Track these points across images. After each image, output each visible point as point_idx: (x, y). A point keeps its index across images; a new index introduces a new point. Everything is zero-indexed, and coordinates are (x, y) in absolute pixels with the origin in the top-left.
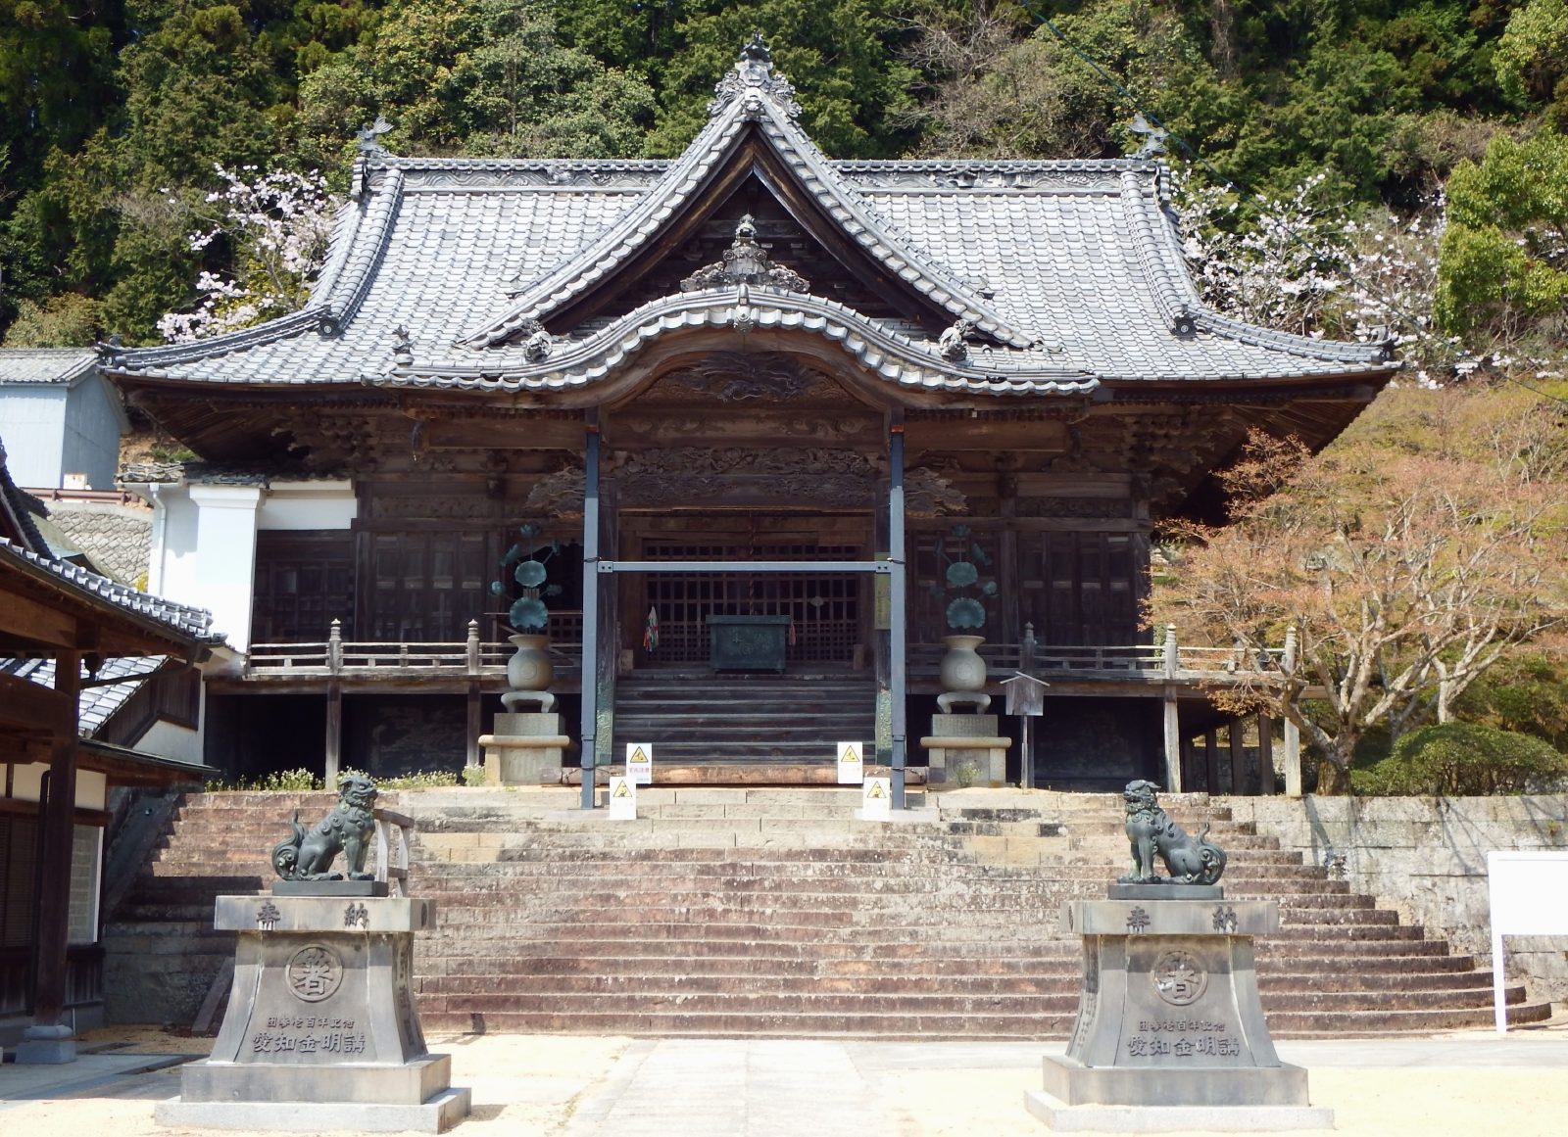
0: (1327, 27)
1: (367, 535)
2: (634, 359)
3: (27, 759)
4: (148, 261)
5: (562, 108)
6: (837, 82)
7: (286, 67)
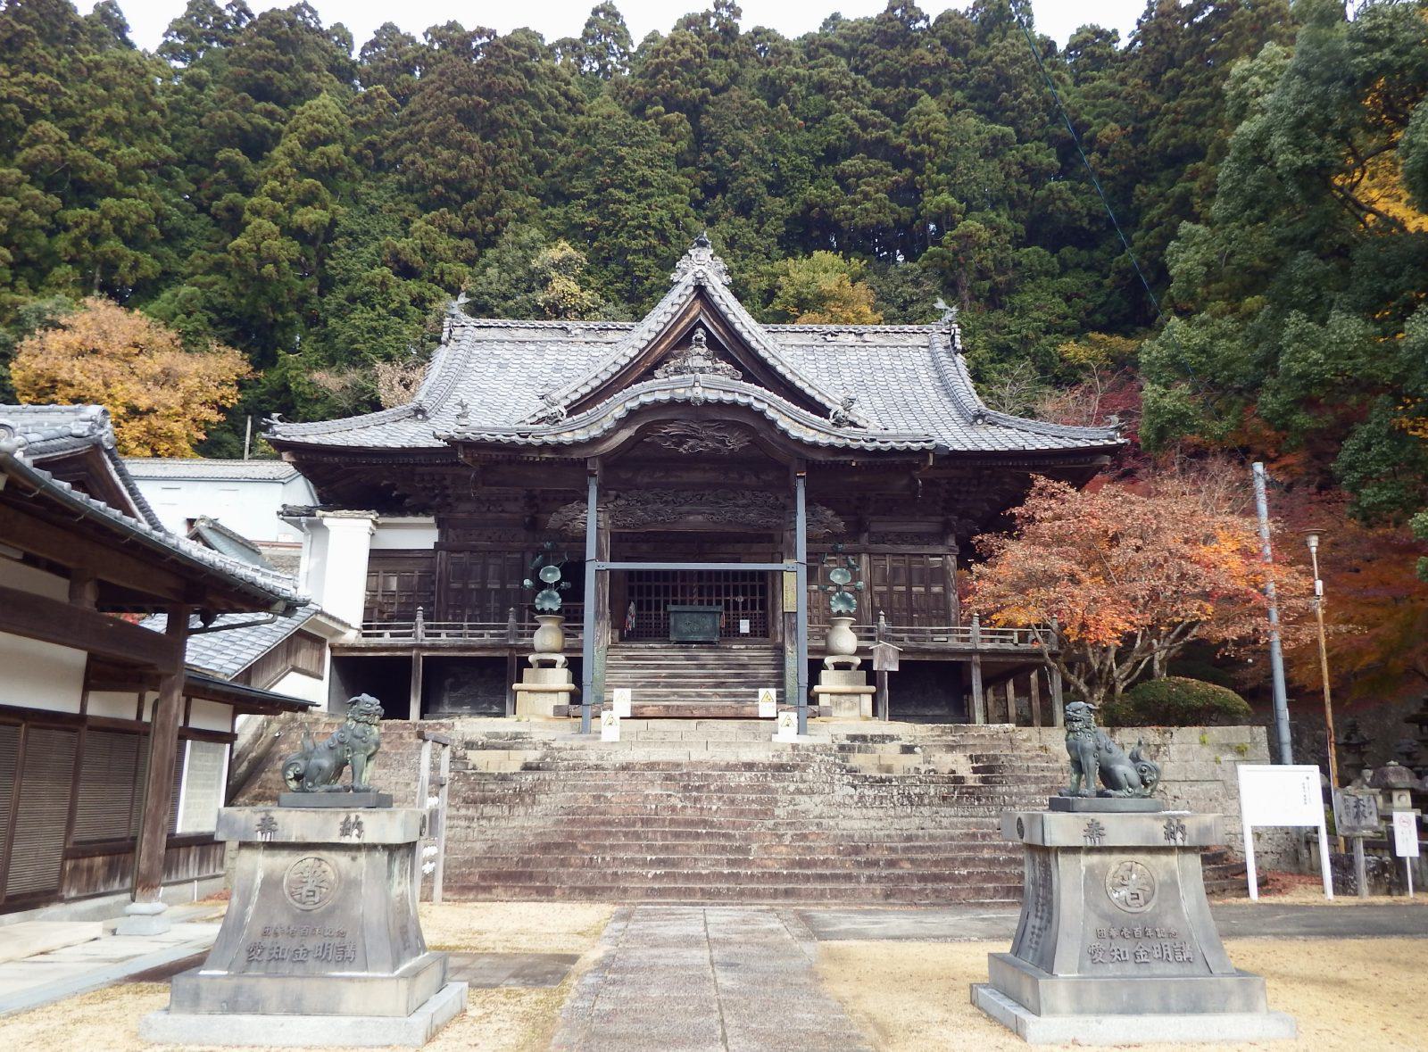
1: (444, 553)
2: (622, 423)
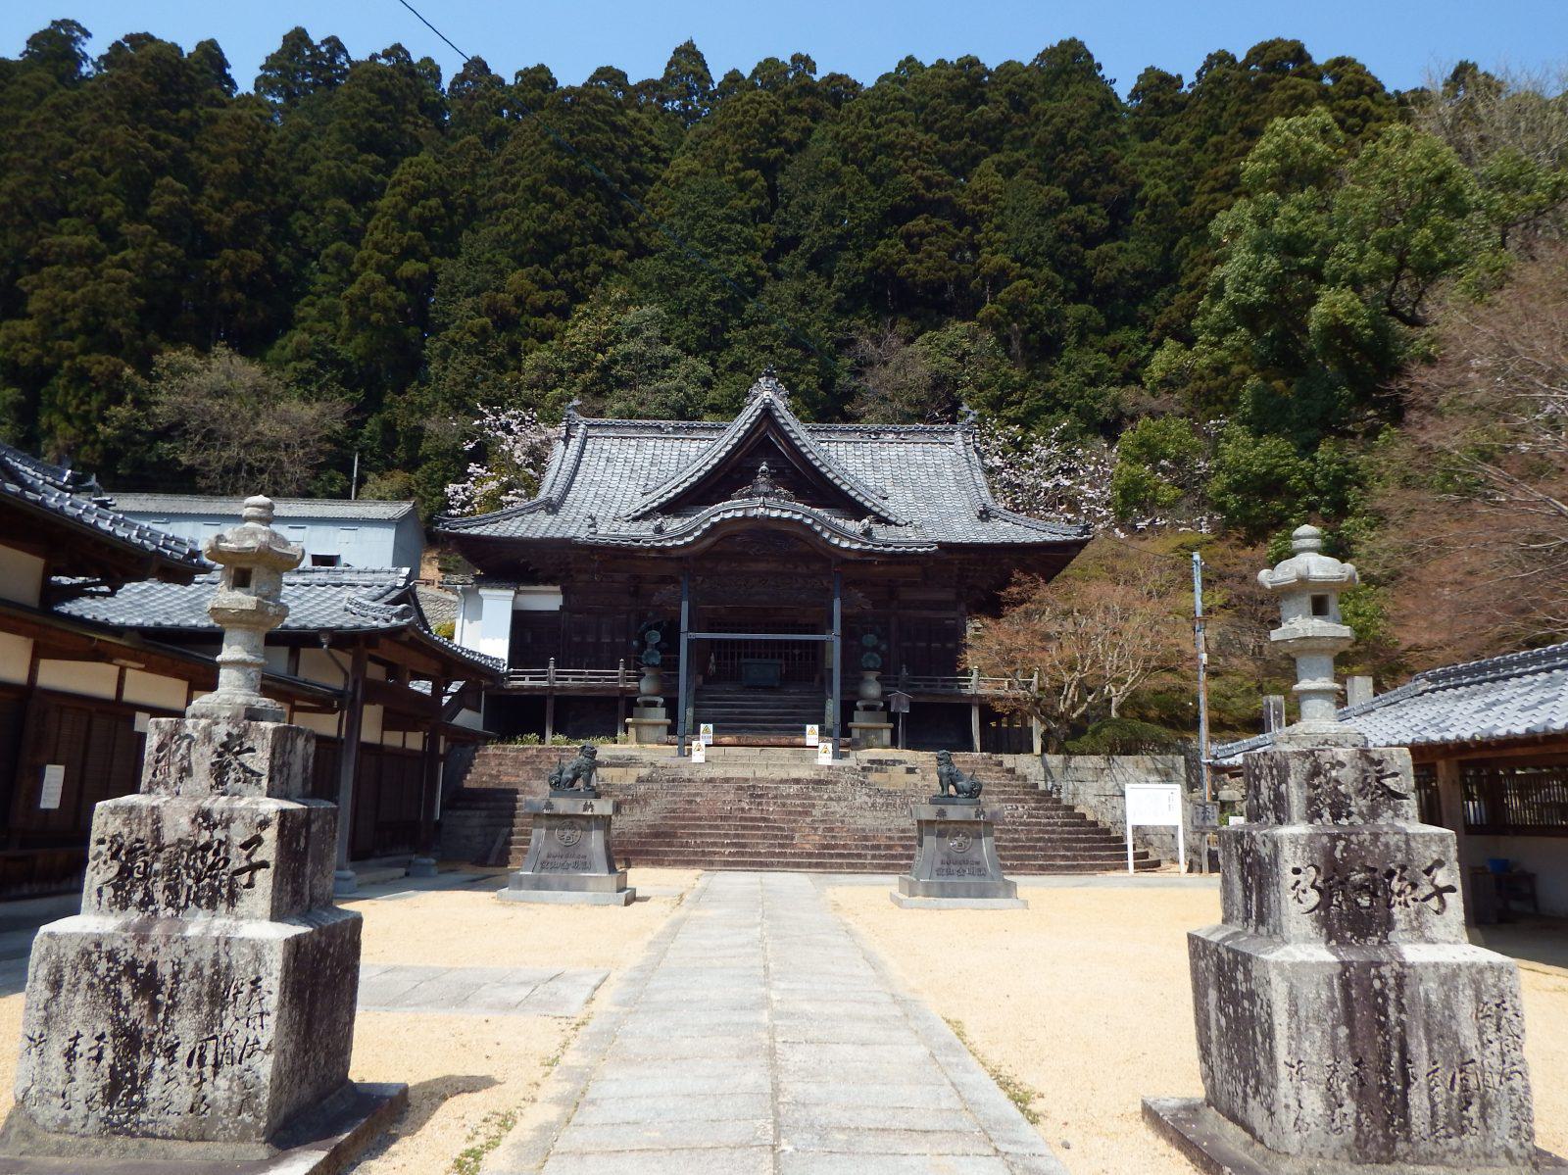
0: (1072, 339)
3: (415, 729)
4: (440, 454)
5: (663, 377)
6: (810, 367)
7: (515, 351)
